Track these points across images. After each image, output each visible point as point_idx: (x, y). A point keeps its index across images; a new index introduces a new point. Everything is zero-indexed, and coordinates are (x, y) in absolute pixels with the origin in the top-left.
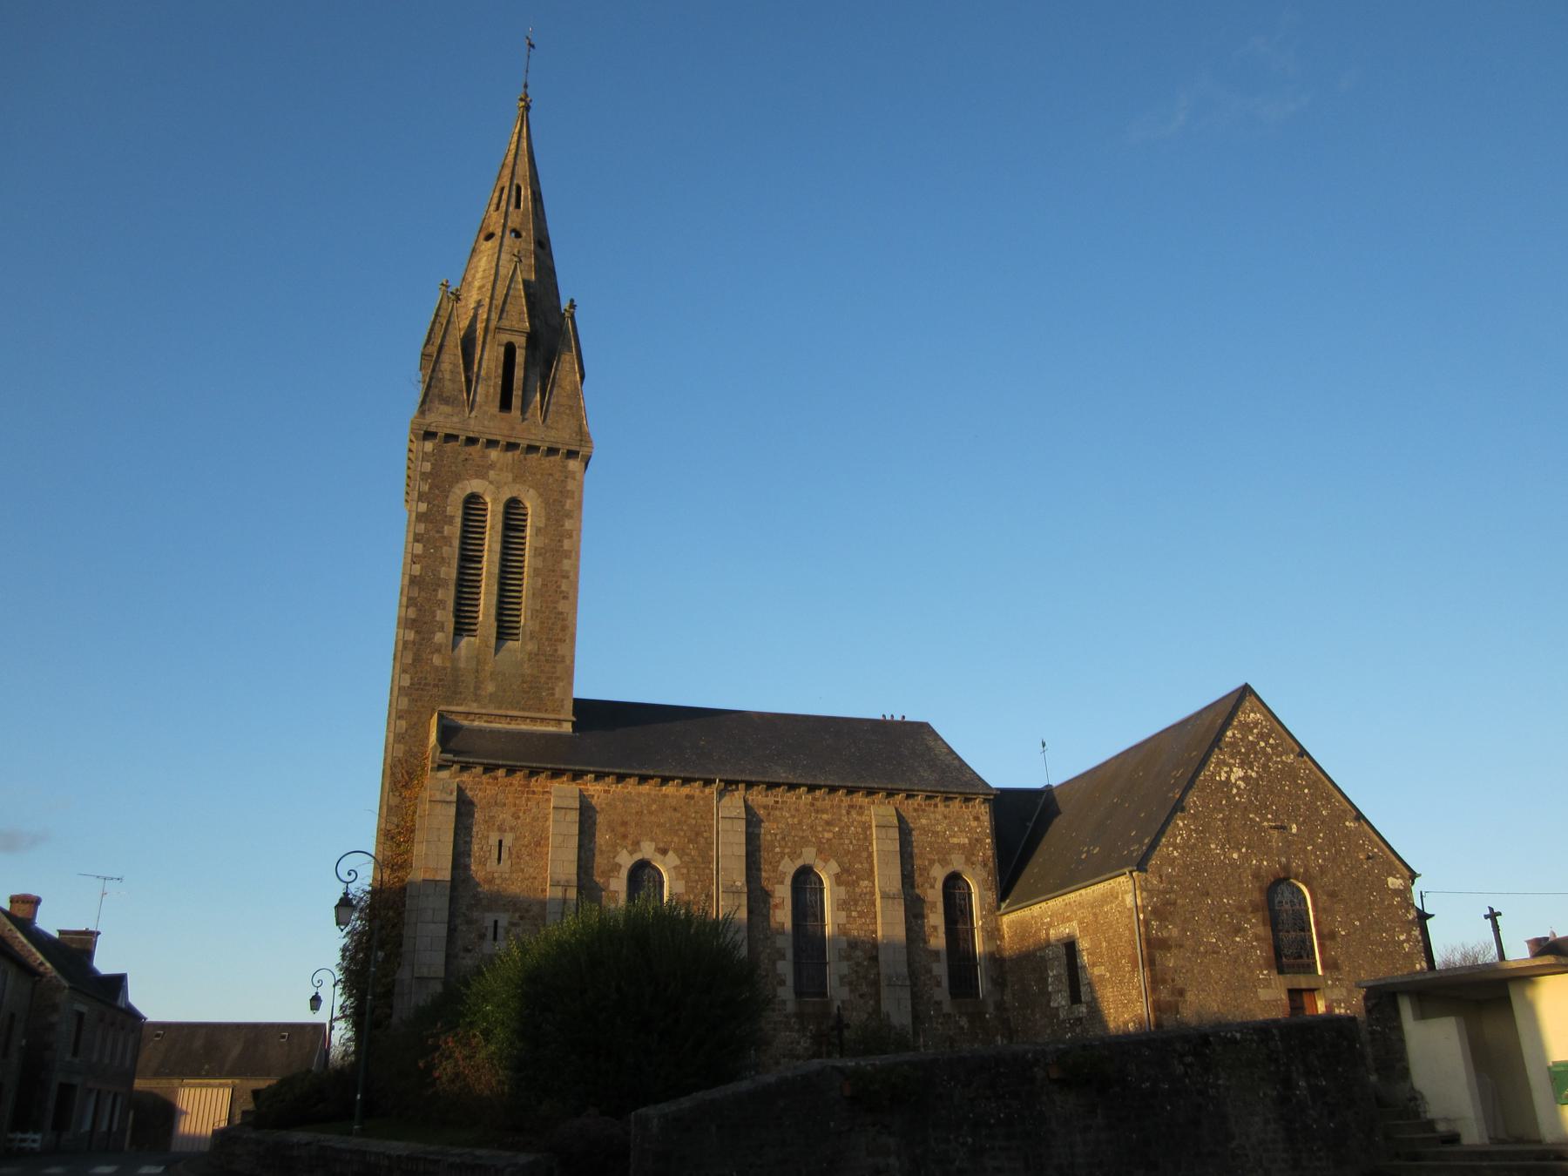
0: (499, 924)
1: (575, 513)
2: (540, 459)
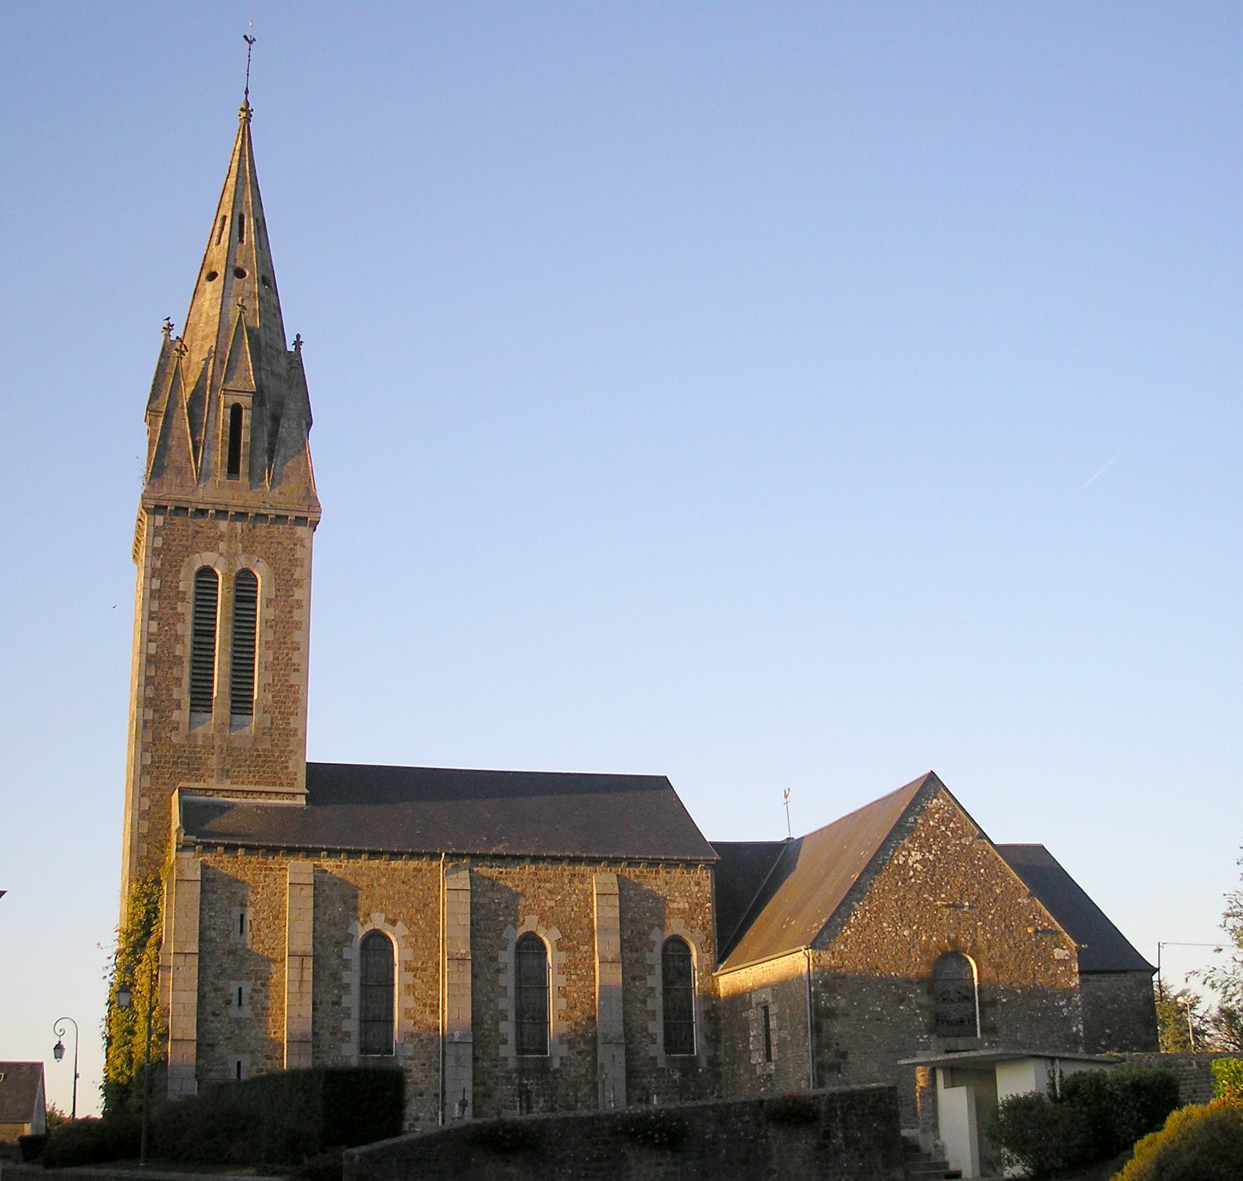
0: (243, 990)
1: (304, 583)
2: (269, 527)
